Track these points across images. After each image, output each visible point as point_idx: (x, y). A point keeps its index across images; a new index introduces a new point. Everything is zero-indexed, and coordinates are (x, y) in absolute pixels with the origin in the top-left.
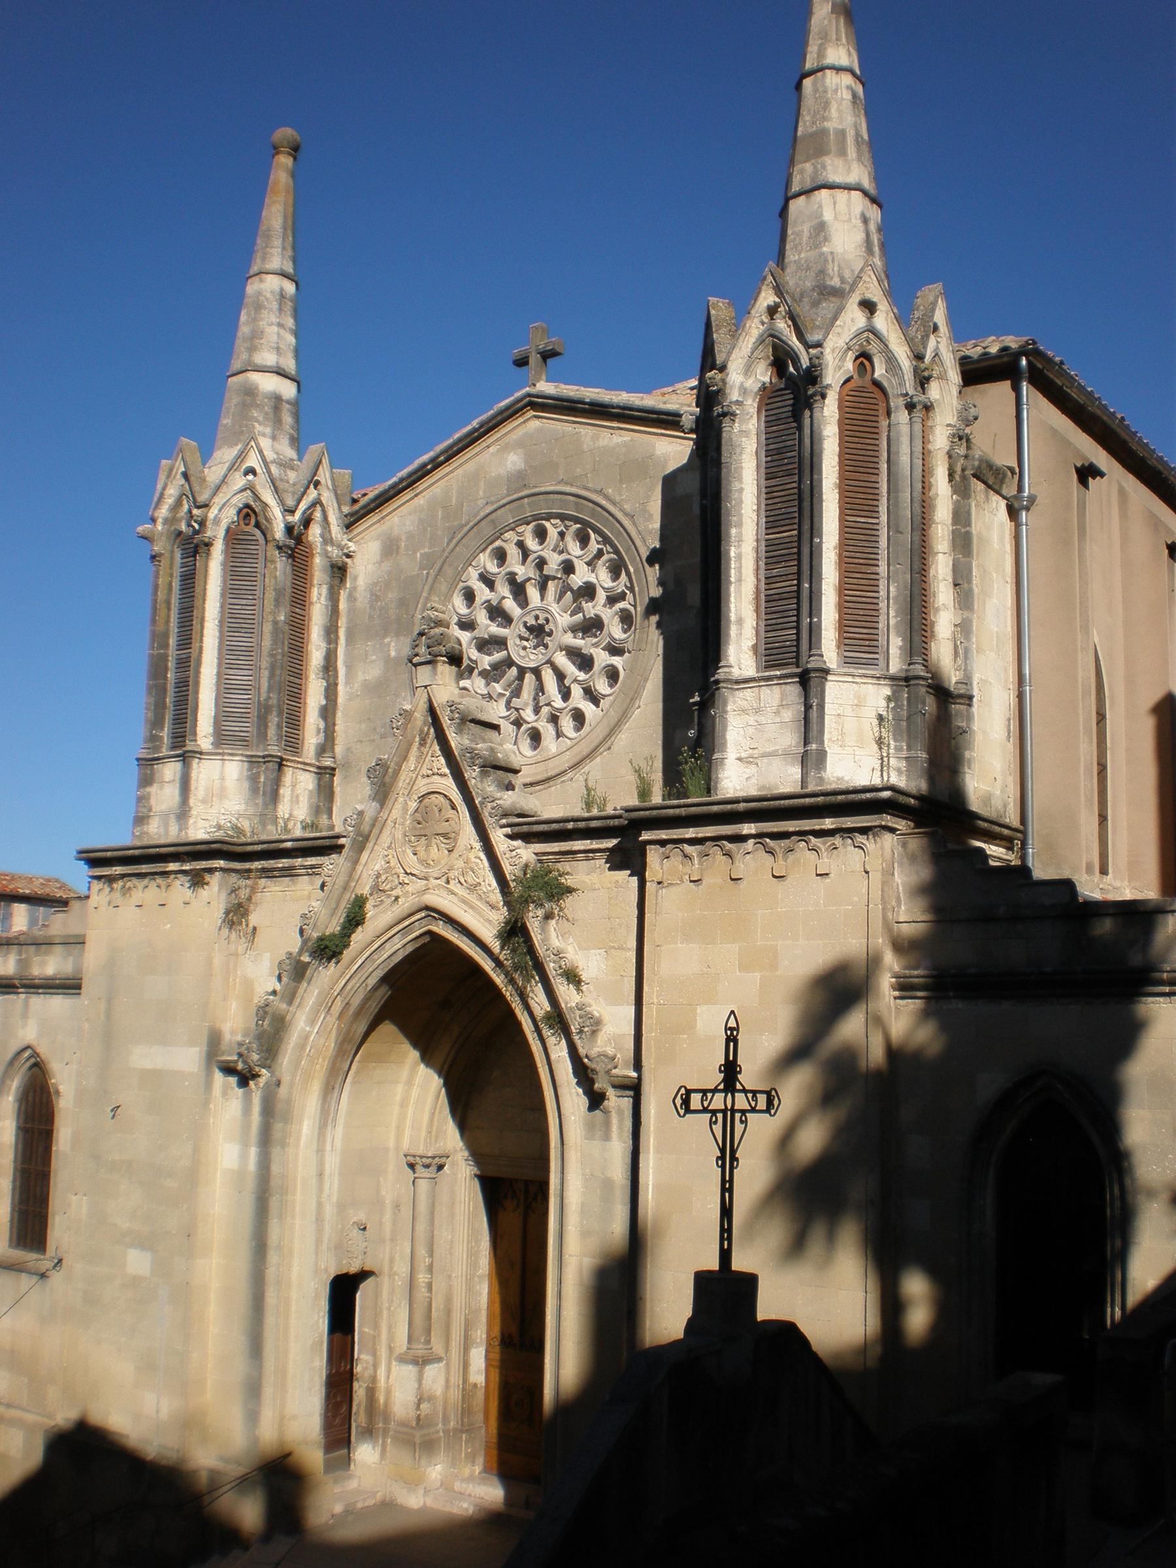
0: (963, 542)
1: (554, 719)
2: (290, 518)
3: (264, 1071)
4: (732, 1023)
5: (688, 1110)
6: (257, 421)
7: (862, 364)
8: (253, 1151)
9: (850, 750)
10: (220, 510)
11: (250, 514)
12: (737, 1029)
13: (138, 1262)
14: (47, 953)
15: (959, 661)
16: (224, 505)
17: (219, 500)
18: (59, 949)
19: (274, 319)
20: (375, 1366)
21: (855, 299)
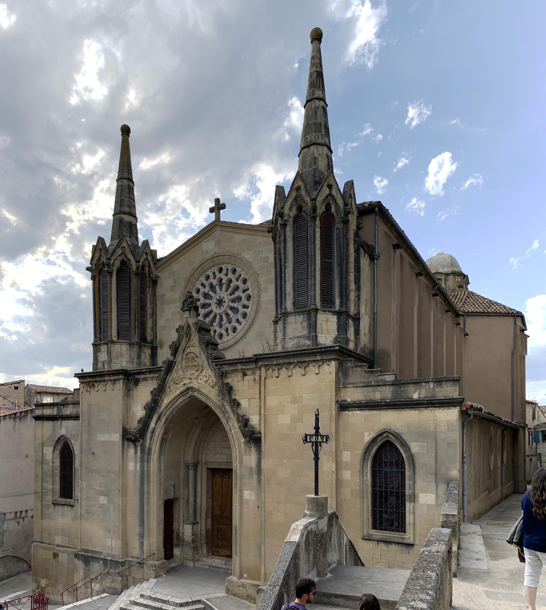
0: (358, 269)
1: (227, 330)
2: (138, 264)
3: (141, 440)
4: (317, 413)
5: (307, 442)
6: (124, 231)
7: (327, 207)
8: (138, 464)
9: (324, 335)
10: (114, 261)
11: (124, 264)
12: (318, 414)
13: (103, 500)
14: (67, 407)
15: (356, 307)
16: (115, 259)
17: (113, 258)
18: (71, 406)
19: (127, 196)
20: (179, 526)
21: (326, 184)
